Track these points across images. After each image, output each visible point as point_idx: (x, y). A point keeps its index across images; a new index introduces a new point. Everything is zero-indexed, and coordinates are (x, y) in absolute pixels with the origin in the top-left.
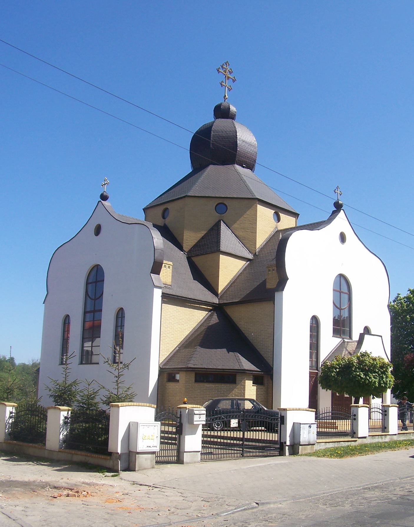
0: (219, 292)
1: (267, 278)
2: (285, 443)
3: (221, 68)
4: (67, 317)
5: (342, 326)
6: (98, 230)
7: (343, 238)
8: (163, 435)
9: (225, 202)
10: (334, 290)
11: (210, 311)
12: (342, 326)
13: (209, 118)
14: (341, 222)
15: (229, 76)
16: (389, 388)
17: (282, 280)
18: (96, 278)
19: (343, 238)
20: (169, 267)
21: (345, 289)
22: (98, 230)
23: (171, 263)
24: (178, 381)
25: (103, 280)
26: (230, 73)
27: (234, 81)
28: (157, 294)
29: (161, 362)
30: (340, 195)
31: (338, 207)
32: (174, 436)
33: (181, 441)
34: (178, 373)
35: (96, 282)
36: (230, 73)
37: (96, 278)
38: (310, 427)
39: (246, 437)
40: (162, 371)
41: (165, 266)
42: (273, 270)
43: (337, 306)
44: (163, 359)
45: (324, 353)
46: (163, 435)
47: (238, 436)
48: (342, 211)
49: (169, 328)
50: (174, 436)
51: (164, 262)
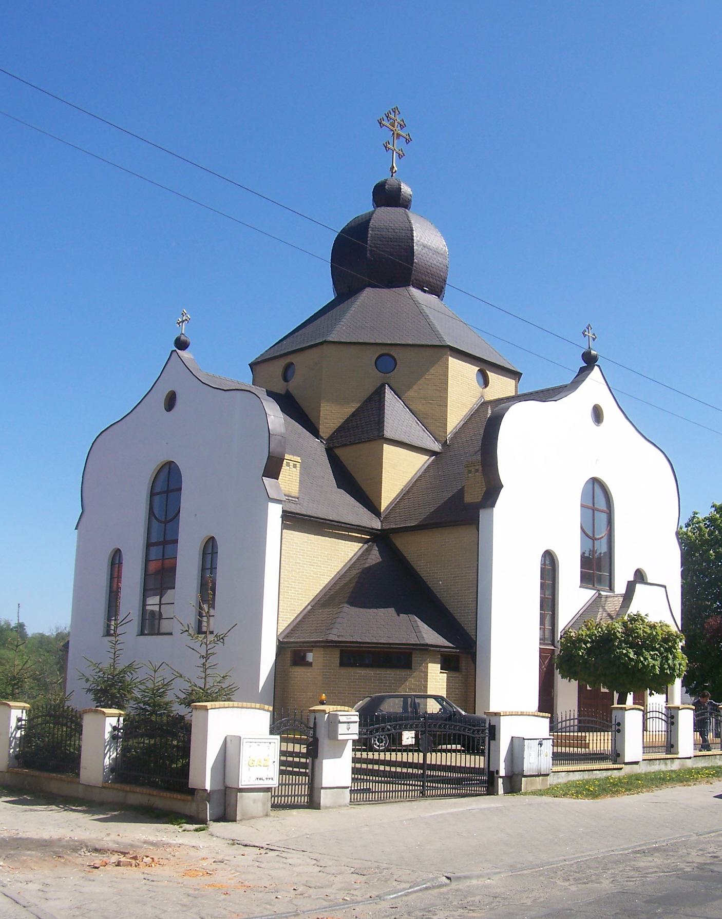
0: (383, 509)
1: (466, 485)
2: (498, 772)
3: (385, 118)
4: (117, 553)
5: (596, 568)
6: (171, 401)
7: (598, 415)
8: (284, 758)
9: (393, 353)
10: (582, 506)
11: (366, 542)
12: (596, 568)
13: (365, 205)
14: (594, 388)
15: (400, 132)
16: (679, 676)
17: (493, 489)
18: (167, 485)
19: (598, 415)
20: (295, 466)
21: (601, 503)
22: (171, 401)
23: (299, 459)
24: (310, 664)
25: (180, 489)
26: (402, 127)
27: (408, 141)
28: (275, 512)
29: (280, 631)
30: (594, 339)
31: (590, 361)
32: (303, 760)
33: (316, 769)
34: (311, 651)
35: (167, 492)
36: (402, 127)
37: (167, 485)
38: (541, 744)
39: (428, 762)
40: (282, 647)
41: (288, 465)
42: (477, 471)
43: (588, 534)
44: (283, 625)
45: (566, 616)
46: (284, 758)
47: (415, 761)
48: (596, 368)
49: (294, 572)
50: (303, 760)
51: (287, 456)
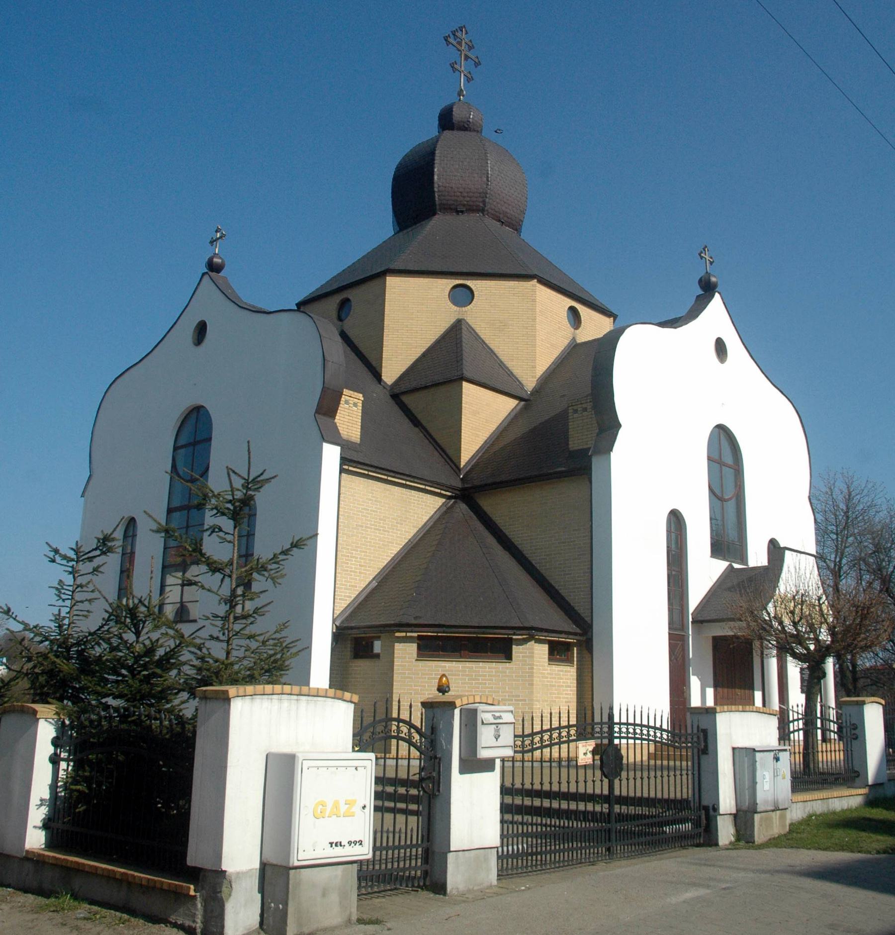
0: (463, 464)
1: (566, 433)
2: (716, 809)
3: (452, 36)
4: (132, 521)
5: (727, 541)
6: (201, 330)
7: (721, 348)
8: (508, 800)
9: (469, 283)
10: (709, 459)
11: (449, 498)
12: (727, 541)
13: (431, 129)
14: (715, 317)
15: (469, 54)
16: (474, 764)
17: (608, 426)
18: (194, 432)
19: (721, 348)
20: (355, 405)
21: (728, 459)
22: (201, 330)
23: (360, 396)
24: (377, 656)
25: (210, 439)
26: (471, 48)
27: (477, 64)
28: (331, 455)
29: (337, 612)
30: (711, 263)
31: (708, 289)
32: (414, 792)
33: (438, 826)
34: (378, 638)
35: (194, 444)
36: (471, 48)
37: (194, 432)
38: (777, 759)
39: (617, 792)
40: (340, 636)
41: (347, 402)
42: (585, 410)
43: (716, 494)
44: (342, 605)
45: (696, 594)
46: (508, 800)
47: (598, 791)
48: (717, 295)
49: (356, 530)
50: (414, 792)
51: (346, 392)
